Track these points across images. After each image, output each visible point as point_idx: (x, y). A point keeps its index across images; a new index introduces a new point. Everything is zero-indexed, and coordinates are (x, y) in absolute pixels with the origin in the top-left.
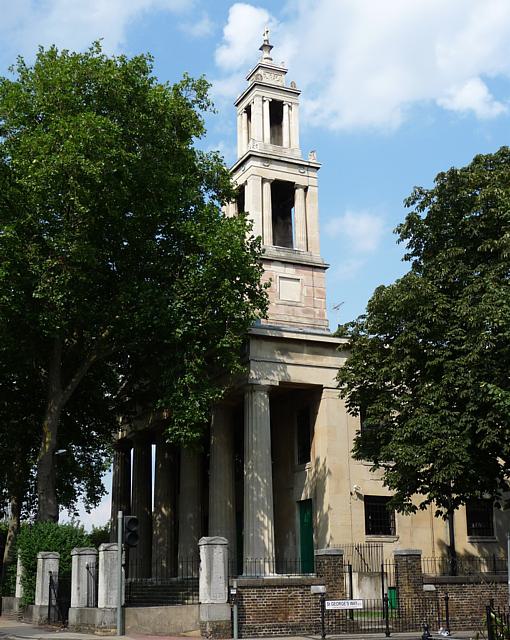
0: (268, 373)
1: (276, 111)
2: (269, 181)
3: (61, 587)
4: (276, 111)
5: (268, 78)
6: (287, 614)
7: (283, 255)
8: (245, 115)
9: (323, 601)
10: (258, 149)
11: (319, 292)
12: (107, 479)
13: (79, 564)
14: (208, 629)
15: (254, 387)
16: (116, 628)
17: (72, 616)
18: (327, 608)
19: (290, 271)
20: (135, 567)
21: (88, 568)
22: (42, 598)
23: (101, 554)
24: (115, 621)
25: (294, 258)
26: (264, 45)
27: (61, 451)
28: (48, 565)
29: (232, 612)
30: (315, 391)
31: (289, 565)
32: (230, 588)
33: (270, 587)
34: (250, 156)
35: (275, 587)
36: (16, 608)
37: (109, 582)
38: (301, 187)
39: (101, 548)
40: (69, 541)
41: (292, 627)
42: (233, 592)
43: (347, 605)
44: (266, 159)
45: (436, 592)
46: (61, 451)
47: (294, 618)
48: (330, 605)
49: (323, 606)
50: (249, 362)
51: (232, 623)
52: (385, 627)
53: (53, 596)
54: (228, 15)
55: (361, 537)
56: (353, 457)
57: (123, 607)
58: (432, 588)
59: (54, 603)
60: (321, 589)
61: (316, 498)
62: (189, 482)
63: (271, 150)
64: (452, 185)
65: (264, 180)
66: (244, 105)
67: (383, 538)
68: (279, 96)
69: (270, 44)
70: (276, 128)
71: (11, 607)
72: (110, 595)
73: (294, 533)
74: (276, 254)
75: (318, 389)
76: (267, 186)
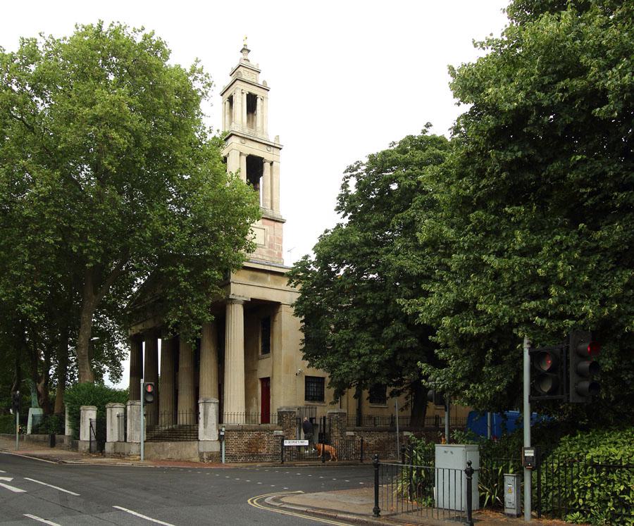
0: (243, 288)
1: (252, 102)
2: (245, 155)
3: (100, 428)
4: (252, 102)
5: (246, 75)
8: (228, 103)
9: (283, 441)
11: (278, 238)
12: (126, 365)
13: (114, 412)
15: (232, 301)
16: (140, 455)
17: (108, 448)
18: (285, 444)
20: (188, 415)
21: (118, 416)
22: (86, 434)
23: (129, 408)
26: (244, 49)
27: (95, 338)
28: (90, 414)
29: (221, 448)
30: (274, 306)
31: (254, 418)
32: (220, 431)
34: (232, 135)
35: (250, 431)
36: (66, 441)
37: (112, 424)
39: (129, 403)
40: (103, 399)
42: (222, 434)
45: (355, 436)
46: (95, 338)
48: (287, 443)
50: (230, 283)
53: (93, 435)
56: (301, 350)
59: (93, 439)
61: (273, 377)
62: (184, 365)
63: (246, 131)
64: (380, 162)
66: (227, 95)
67: (316, 403)
68: (254, 91)
69: (248, 48)
70: (251, 115)
71: (62, 441)
72: (137, 433)
73: (257, 398)
75: (278, 305)
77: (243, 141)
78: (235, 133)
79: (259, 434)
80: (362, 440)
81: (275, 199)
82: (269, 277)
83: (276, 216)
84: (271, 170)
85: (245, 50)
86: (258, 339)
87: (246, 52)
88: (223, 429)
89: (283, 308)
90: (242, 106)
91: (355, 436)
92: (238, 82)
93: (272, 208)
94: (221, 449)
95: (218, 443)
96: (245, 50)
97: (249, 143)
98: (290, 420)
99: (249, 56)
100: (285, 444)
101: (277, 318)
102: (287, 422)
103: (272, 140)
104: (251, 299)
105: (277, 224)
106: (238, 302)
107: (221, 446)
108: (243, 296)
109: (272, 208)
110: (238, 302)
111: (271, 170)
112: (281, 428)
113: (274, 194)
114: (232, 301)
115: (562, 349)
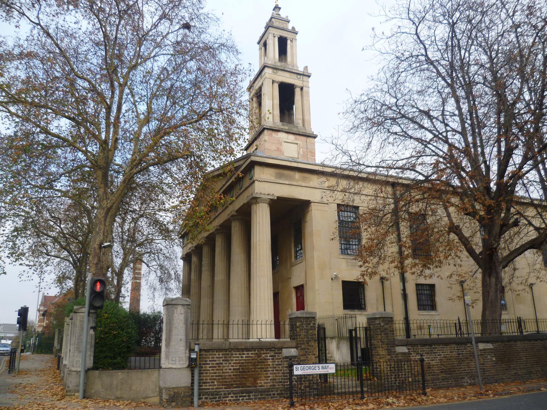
1: (283, 43)
2: (277, 82)
4: (283, 43)
5: (276, 23)
6: (256, 379)
7: (287, 128)
8: (263, 48)
9: (291, 367)
10: (270, 62)
11: (311, 152)
14: (165, 397)
18: (296, 373)
19: (291, 137)
24: (78, 386)
25: (295, 130)
28: (355, 362)
29: (193, 380)
33: (238, 350)
35: (243, 350)
38: (299, 87)
41: (262, 392)
42: (194, 356)
43: (318, 369)
44: (275, 68)
45: (409, 353)
47: (264, 383)
48: (298, 370)
49: (291, 371)
51: (193, 389)
52: (359, 389)
54: (292, 109)
55: (338, 309)
57: (87, 371)
58: (404, 349)
60: (293, 352)
65: (273, 82)
67: (356, 312)
68: (284, 34)
74: (282, 127)
76: (276, 86)
77: (275, 71)
78: (267, 65)
79: (259, 355)
80: (422, 361)
81: (306, 118)
82: (297, 175)
83: (308, 132)
84: (302, 94)
85: (277, 8)
86: (291, 245)
87: (278, 9)
88: (197, 348)
89: (313, 207)
90: (274, 46)
91: (409, 353)
92: (270, 28)
93: (304, 125)
94: (193, 383)
95: (188, 373)
96: (277, 8)
97: (280, 73)
98: (307, 330)
99: (280, 12)
100: (296, 373)
101: (308, 218)
102: (303, 333)
103: (301, 69)
104: (277, 197)
105: (309, 139)
106: (263, 201)
107: (193, 377)
108: (268, 195)
109: (304, 125)
110: (263, 201)
111: (302, 94)
112: (294, 344)
113: (306, 113)
114: (255, 200)
115: (273, 400)
